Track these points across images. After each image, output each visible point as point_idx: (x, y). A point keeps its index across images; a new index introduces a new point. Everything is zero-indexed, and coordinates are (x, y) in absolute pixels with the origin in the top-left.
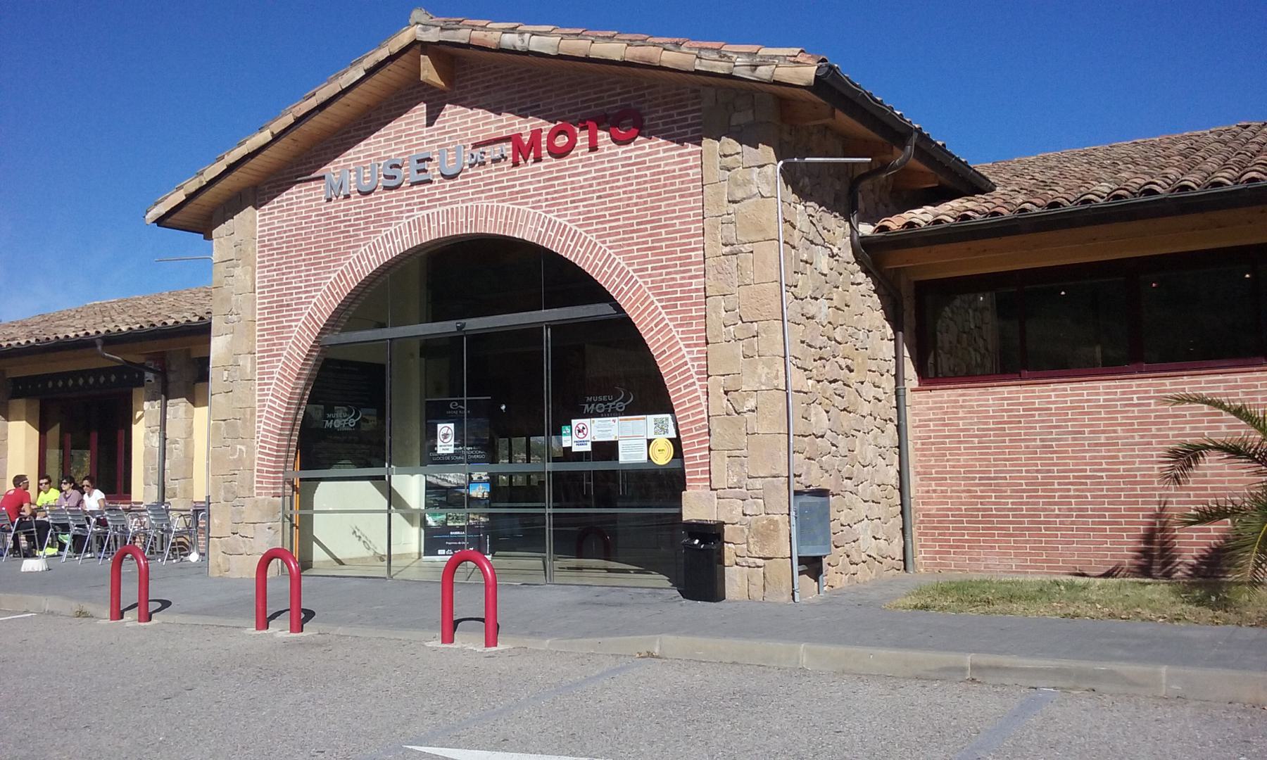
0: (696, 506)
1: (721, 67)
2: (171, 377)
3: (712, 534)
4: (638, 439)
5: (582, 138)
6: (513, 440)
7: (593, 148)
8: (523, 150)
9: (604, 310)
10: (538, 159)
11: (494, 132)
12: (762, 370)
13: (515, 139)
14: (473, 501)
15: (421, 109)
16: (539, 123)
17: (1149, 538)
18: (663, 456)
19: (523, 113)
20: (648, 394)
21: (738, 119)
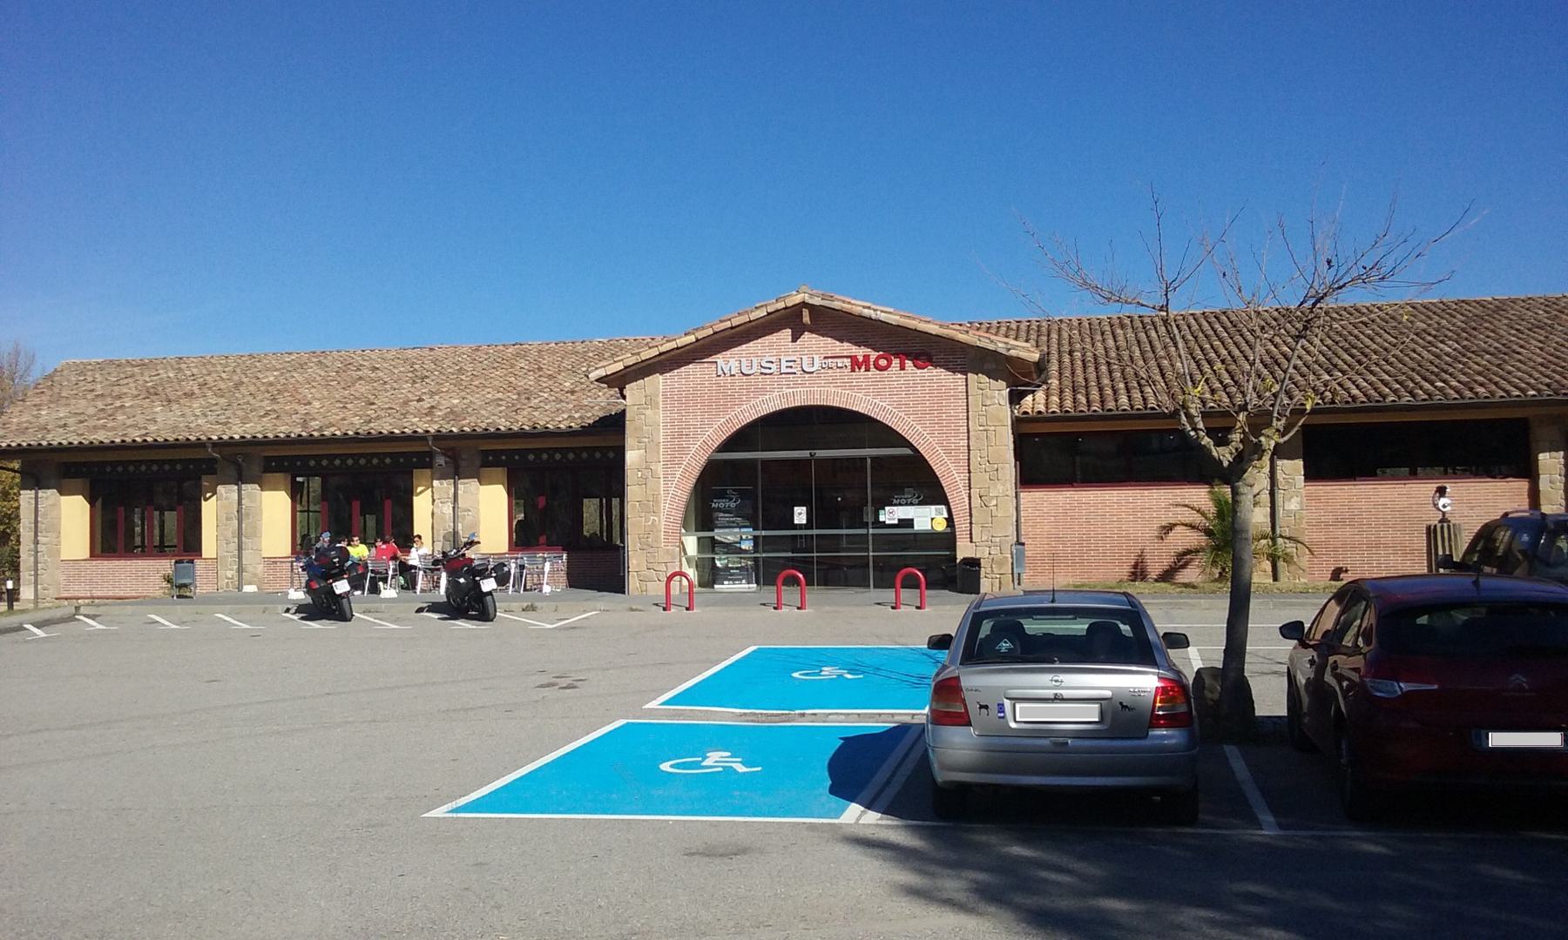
0: (964, 551)
1: (991, 347)
2: (463, 464)
3: (974, 563)
4: (927, 518)
5: (896, 362)
6: (41, 493)
7: (902, 368)
8: (855, 364)
9: (908, 451)
10: (867, 370)
11: (838, 351)
12: (1000, 487)
13: (853, 359)
14: (741, 551)
15: (788, 332)
16: (868, 351)
17: (1135, 566)
18: (941, 526)
19: (858, 344)
20: (933, 493)
21: (987, 366)
